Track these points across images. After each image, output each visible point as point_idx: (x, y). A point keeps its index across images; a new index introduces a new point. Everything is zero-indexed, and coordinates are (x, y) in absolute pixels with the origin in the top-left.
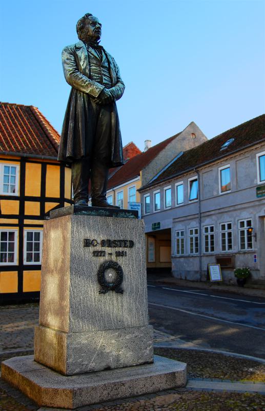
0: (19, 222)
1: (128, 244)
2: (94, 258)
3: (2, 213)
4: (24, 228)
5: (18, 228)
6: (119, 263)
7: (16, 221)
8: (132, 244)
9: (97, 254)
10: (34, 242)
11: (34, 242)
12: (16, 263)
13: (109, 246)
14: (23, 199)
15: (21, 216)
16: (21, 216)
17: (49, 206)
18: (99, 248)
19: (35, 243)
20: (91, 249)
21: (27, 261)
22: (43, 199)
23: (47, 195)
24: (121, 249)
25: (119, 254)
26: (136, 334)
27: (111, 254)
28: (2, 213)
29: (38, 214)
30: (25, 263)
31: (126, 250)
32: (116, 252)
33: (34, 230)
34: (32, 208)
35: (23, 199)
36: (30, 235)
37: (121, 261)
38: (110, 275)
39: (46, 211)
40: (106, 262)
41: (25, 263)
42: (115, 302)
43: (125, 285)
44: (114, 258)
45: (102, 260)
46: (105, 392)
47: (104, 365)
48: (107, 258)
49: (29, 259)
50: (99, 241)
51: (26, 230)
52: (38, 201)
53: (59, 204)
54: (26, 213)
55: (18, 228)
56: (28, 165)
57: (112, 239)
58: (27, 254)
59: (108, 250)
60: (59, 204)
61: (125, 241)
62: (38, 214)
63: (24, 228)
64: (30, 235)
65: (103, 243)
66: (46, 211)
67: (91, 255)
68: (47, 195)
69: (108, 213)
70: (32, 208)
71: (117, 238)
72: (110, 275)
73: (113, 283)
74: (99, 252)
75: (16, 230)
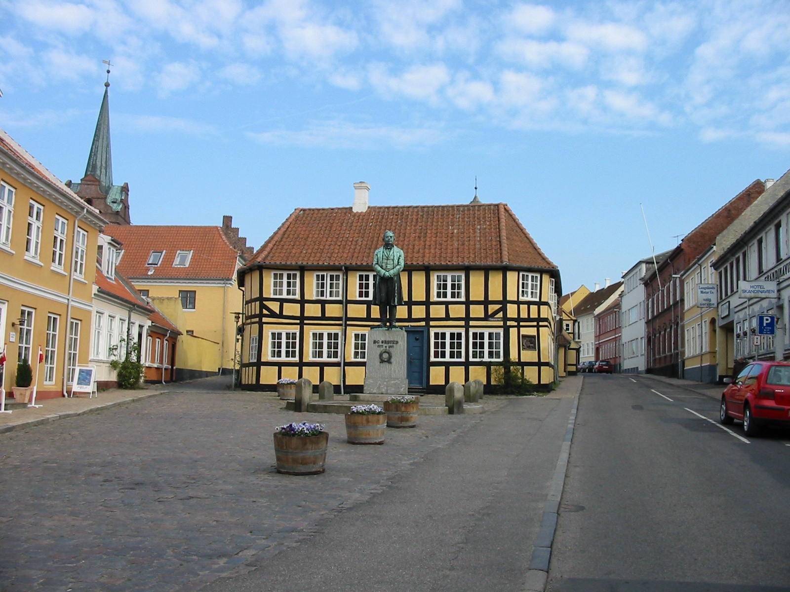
2: (378, 348)
4: (470, 329)
7: (463, 323)
8: (397, 342)
9: (379, 346)
10: (494, 341)
11: (456, 341)
12: (463, 359)
13: (385, 343)
14: (468, 303)
15: (467, 318)
16: (467, 318)
17: (492, 308)
18: (381, 344)
19: (454, 340)
21: (473, 358)
22: (486, 302)
24: (392, 345)
30: (471, 359)
31: (394, 345)
34: (477, 311)
37: (391, 350)
38: (385, 356)
41: (471, 359)
43: (392, 360)
47: (380, 392)
50: (380, 341)
51: (471, 331)
52: (509, 301)
53: (501, 306)
57: (387, 340)
58: (461, 348)
59: (384, 345)
60: (501, 306)
63: (470, 329)
64: (475, 334)
66: (489, 313)
70: (477, 311)
72: (385, 356)
75: (462, 331)
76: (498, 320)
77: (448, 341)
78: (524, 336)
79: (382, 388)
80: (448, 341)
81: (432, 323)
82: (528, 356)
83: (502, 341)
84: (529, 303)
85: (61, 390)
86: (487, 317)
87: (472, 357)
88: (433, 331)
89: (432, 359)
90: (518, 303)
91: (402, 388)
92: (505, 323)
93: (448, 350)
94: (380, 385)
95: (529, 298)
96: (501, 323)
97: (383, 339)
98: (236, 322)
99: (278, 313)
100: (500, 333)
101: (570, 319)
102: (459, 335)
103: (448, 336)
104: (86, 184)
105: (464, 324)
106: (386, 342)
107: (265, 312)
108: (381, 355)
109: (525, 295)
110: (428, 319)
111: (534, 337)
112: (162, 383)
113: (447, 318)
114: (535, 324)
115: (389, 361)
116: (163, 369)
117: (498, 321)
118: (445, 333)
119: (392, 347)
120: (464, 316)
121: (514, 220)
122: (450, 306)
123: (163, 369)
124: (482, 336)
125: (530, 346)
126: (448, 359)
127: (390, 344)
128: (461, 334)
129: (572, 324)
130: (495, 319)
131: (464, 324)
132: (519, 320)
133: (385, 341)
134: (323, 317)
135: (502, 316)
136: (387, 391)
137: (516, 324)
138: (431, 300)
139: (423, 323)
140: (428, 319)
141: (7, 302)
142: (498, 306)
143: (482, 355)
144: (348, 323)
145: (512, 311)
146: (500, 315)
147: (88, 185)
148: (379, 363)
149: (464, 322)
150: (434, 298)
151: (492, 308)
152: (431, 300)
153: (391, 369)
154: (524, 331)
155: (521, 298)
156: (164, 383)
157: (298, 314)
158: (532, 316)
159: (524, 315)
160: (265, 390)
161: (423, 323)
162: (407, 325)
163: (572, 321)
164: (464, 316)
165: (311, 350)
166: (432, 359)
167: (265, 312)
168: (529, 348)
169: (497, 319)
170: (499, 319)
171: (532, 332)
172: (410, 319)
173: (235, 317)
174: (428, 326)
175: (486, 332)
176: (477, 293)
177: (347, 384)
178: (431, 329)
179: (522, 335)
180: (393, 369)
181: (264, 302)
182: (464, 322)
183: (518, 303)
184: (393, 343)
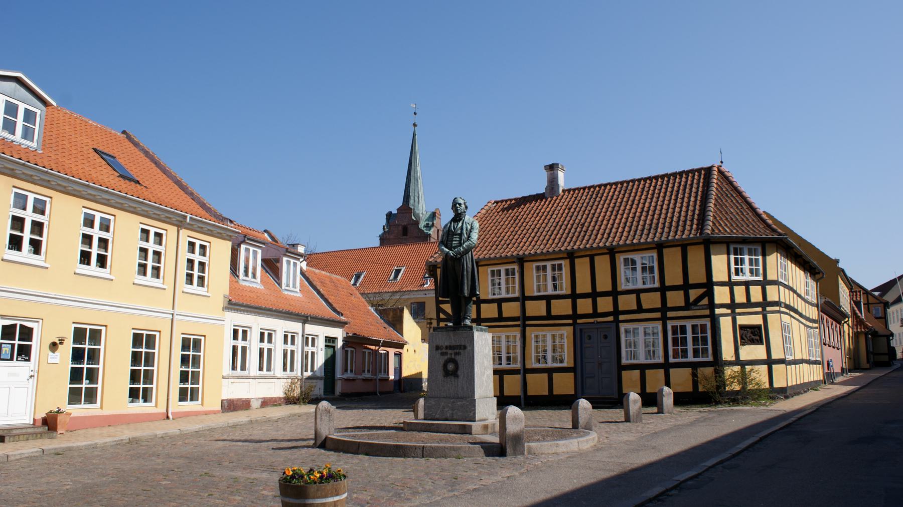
0: (614, 318)
1: (462, 347)
3: (643, 308)
5: (661, 322)
6: (456, 359)
7: (658, 315)
8: (465, 347)
9: (443, 354)
13: (450, 349)
15: (664, 308)
16: (664, 308)
17: (694, 294)
18: (444, 350)
20: (440, 351)
22: (686, 287)
23: (692, 281)
24: (458, 351)
25: (456, 354)
26: (464, 402)
27: (451, 354)
28: (643, 308)
29: (682, 304)
30: (671, 360)
32: (455, 353)
33: (679, 323)
34: (675, 298)
35: (663, 289)
36: (674, 328)
37: (458, 358)
38: (451, 367)
39: (692, 300)
40: (448, 359)
41: (671, 360)
42: (453, 382)
43: (459, 373)
44: (453, 356)
45: (446, 357)
46: (423, 427)
48: (449, 356)
49: (676, 355)
50: (444, 347)
51: (670, 324)
53: (705, 290)
54: (669, 305)
55: (661, 322)
56: (665, 251)
59: (450, 351)
60: (705, 290)
61: (460, 346)
62: (682, 304)
64: (674, 328)
65: (447, 347)
66: (692, 300)
67: (439, 355)
68: (692, 281)
69: (453, 329)
70: (675, 298)
71: (455, 344)
73: (452, 371)
74: (443, 353)
76: (703, 308)
77: (689, 335)
78: (743, 327)
79: (447, 411)
80: (689, 335)
81: (621, 317)
82: (756, 352)
83: (709, 334)
84: (747, 284)
85: (165, 411)
86: (688, 306)
87: (672, 357)
88: (623, 327)
89: (624, 361)
90: (731, 284)
91: (471, 412)
92: (712, 312)
93: (690, 347)
94: (444, 407)
95: (747, 277)
96: (707, 312)
97: (447, 344)
98: (428, 329)
99: (441, 314)
100: (706, 325)
101: (878, 302)
102: (703, 327)
103: (689, 330)
104: (401, 213)
105: (660, 316)
106: (450, 347)
107: (442, 316)
108: (445, 366)
109: (741, 274)
110: (616, 312)
111: (759, 327)
112: (376, 394)
113: (640, 309)
114: (759, 309)
115: (454, 373)
116: (378, 380)
117: (703, 309)
118: (685, 326)
119: (458, 354)
120: (659, 306)
121: (731, 183)
122: (641, 295)
123: (378, 380)
124: (683, 329)
125: (753, 339)
126: (691, 358)
127: (455, 351)
128: (706, 325)
129: (883, 309)
130: (698, 308)
131: (660, 316)
132: (733, 306)
133: (450, 346)
134: (549, 316)
135: (707, 303)
136: (453, 416)
137: (729, 311)
138: (619, 289)
139: (611, 318)
140: (616, 312)
141: (41, 320)
142: (701, 291)
143: (685, 353)
144: (527, 322)
145: (721, 295)
146: (705, 301)
147: (403, 213)
148: (442, 377)
149: (660, 313)
150: (623, 286)
151: (694, 294)
152: (619, 289)
153: (458, 385)
154: (742, 320)
155: (734, 278)
156: (378, 394)
157: (570, 312)
158: (753, 300)
159: (740, 297)
160: (404, 407)
161: (611, 318)
162: (593, 321)
163: (882, 305)
164: (659, 306)
165: (533, 354)
166: (624, 361)
167: (442, 316)
168: (753, 342)
169: (701, 307)
170: (704, 307)
171: (757, 320)
172: (595, 314)
173: (428, 323)
174: (617, 322)
175: (689, 324)
176: (674, 276)
177: (529, 393)
178: (620, 324)
179: (739, 325)
180: (459, 384)
181: (440, 305)
182: (660, 313)
183: (731, 284)
184: (460, 349)
